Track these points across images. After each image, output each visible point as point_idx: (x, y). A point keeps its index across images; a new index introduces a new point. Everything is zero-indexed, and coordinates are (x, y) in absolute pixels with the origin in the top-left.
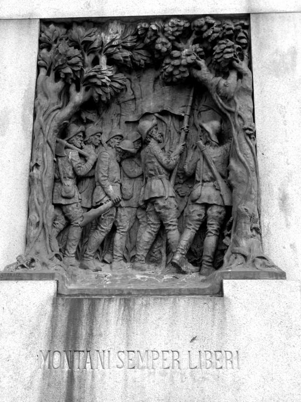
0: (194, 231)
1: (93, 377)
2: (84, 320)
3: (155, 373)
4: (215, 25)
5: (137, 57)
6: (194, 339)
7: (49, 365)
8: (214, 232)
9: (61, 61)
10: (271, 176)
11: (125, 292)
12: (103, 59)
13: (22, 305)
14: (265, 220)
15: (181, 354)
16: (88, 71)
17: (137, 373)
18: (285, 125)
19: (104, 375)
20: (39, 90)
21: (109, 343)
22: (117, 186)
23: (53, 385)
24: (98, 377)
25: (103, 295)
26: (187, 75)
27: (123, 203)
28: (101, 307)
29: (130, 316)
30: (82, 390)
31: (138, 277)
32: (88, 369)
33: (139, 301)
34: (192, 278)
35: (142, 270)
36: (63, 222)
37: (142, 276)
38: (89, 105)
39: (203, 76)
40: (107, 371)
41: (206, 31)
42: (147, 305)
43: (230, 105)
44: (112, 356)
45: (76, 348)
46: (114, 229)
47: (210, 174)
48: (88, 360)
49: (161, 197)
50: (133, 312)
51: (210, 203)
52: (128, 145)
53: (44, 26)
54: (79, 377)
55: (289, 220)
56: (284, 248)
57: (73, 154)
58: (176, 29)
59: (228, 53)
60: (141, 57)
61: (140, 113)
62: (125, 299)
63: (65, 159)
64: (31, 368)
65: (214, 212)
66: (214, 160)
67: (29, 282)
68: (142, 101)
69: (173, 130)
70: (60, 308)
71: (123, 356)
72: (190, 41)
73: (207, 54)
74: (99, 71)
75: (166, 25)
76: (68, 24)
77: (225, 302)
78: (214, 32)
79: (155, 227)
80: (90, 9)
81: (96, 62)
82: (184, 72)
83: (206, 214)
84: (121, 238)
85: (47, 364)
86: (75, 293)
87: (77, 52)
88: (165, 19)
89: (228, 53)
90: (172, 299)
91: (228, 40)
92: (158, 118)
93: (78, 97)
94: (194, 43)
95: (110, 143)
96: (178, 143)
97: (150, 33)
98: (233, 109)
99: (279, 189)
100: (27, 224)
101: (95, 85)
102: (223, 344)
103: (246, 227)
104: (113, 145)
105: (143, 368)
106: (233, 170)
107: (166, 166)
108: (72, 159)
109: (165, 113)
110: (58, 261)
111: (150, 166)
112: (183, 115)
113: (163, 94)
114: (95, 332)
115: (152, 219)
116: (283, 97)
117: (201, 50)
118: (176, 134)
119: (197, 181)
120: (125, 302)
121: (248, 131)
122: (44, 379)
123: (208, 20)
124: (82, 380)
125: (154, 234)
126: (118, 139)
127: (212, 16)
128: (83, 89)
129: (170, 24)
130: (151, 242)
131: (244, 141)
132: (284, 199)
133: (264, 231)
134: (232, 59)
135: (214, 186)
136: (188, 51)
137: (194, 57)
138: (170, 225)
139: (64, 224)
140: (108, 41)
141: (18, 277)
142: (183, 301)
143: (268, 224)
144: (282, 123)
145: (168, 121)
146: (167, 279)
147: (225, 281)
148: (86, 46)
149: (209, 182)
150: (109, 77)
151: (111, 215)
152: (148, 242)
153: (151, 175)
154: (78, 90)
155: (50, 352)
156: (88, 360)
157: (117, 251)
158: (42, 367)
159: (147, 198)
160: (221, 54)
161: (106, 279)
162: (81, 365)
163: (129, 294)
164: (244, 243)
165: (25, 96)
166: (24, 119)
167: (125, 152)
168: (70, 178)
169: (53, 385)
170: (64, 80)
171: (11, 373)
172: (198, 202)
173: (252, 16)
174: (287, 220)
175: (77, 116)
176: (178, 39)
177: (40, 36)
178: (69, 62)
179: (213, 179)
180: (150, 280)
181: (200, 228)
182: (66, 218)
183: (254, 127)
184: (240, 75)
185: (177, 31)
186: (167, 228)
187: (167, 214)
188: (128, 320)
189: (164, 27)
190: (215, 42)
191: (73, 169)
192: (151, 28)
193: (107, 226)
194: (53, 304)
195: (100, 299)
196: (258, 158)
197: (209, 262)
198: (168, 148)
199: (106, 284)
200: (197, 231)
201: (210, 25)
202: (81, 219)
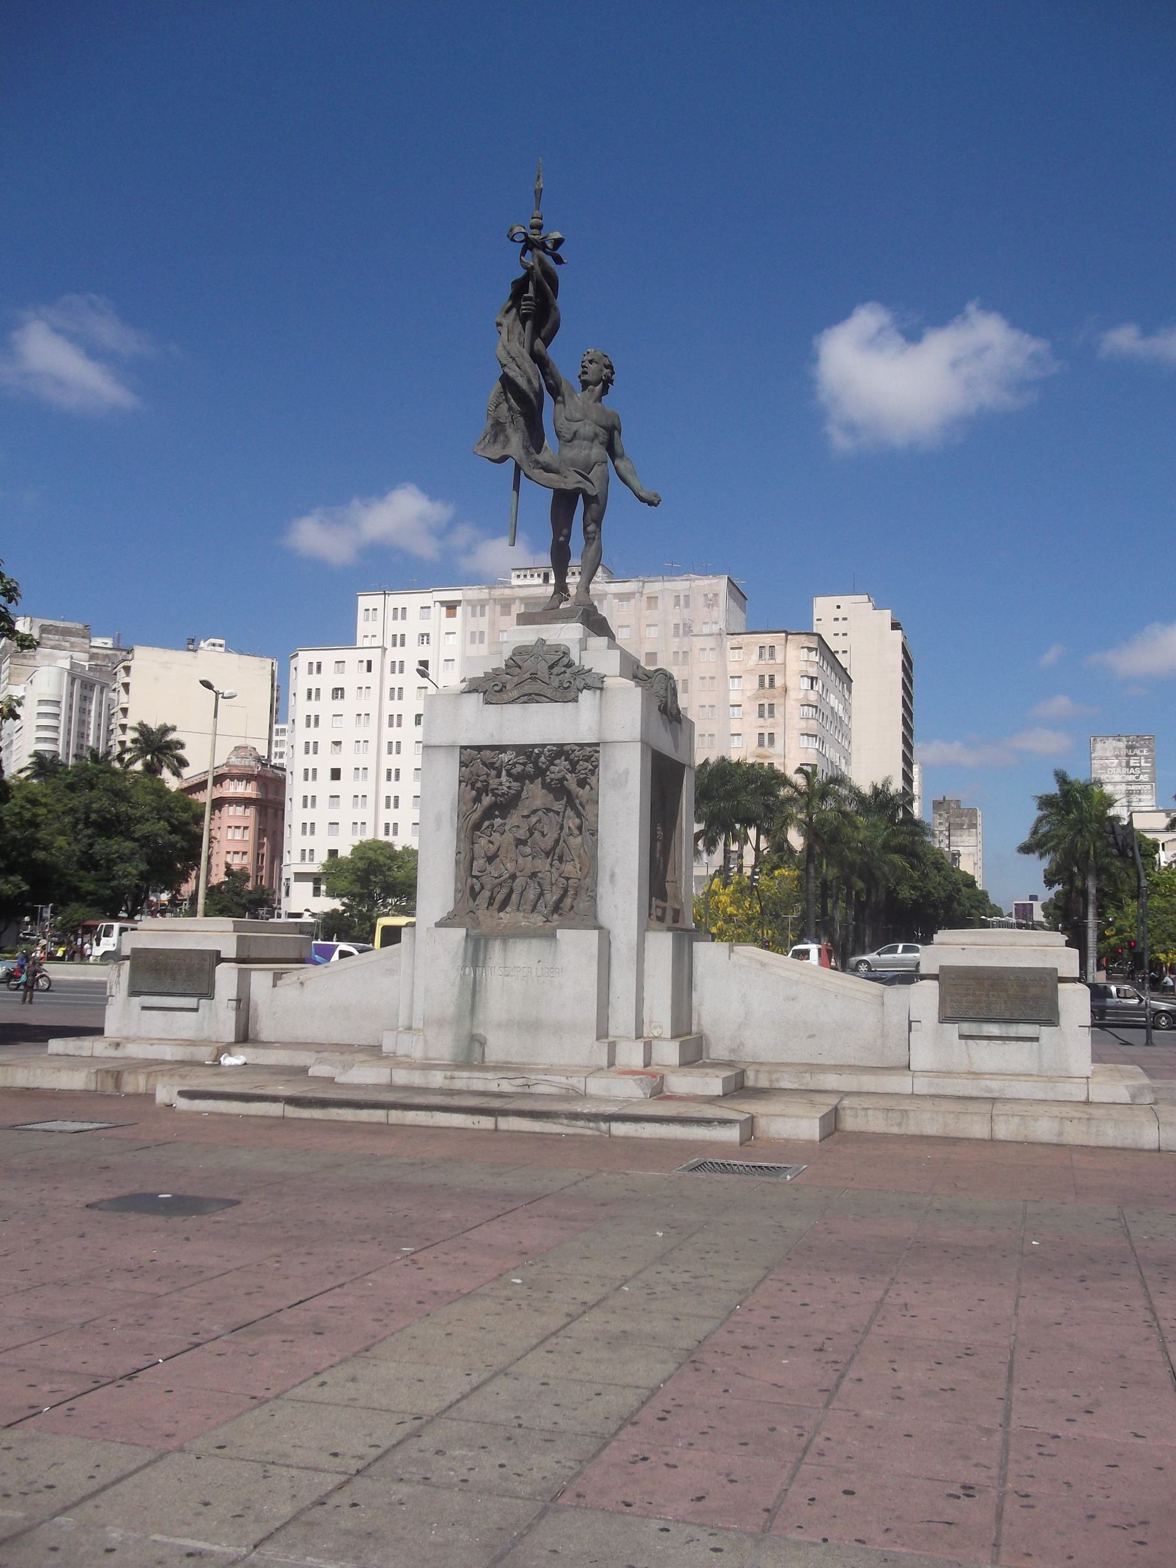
2: (482, 951)
12: (504, 773)
14: (600, 890)
27: (518, 874)
33: (511, 941)
38: (493, 806)
46: (512, 891)
52: (522, 834)
57: (483, 841)
60: (530, 768)
64: (455, 975)
74: (501, 784)
81: (499, 776)
88: (544, 746)
93: (487, 800)
132: (612, 876)
155: (464, 967)
167: (518, 839)
175: (488, 814)
188: (505, 951)
193: (505, 891)
201: (573, 751)
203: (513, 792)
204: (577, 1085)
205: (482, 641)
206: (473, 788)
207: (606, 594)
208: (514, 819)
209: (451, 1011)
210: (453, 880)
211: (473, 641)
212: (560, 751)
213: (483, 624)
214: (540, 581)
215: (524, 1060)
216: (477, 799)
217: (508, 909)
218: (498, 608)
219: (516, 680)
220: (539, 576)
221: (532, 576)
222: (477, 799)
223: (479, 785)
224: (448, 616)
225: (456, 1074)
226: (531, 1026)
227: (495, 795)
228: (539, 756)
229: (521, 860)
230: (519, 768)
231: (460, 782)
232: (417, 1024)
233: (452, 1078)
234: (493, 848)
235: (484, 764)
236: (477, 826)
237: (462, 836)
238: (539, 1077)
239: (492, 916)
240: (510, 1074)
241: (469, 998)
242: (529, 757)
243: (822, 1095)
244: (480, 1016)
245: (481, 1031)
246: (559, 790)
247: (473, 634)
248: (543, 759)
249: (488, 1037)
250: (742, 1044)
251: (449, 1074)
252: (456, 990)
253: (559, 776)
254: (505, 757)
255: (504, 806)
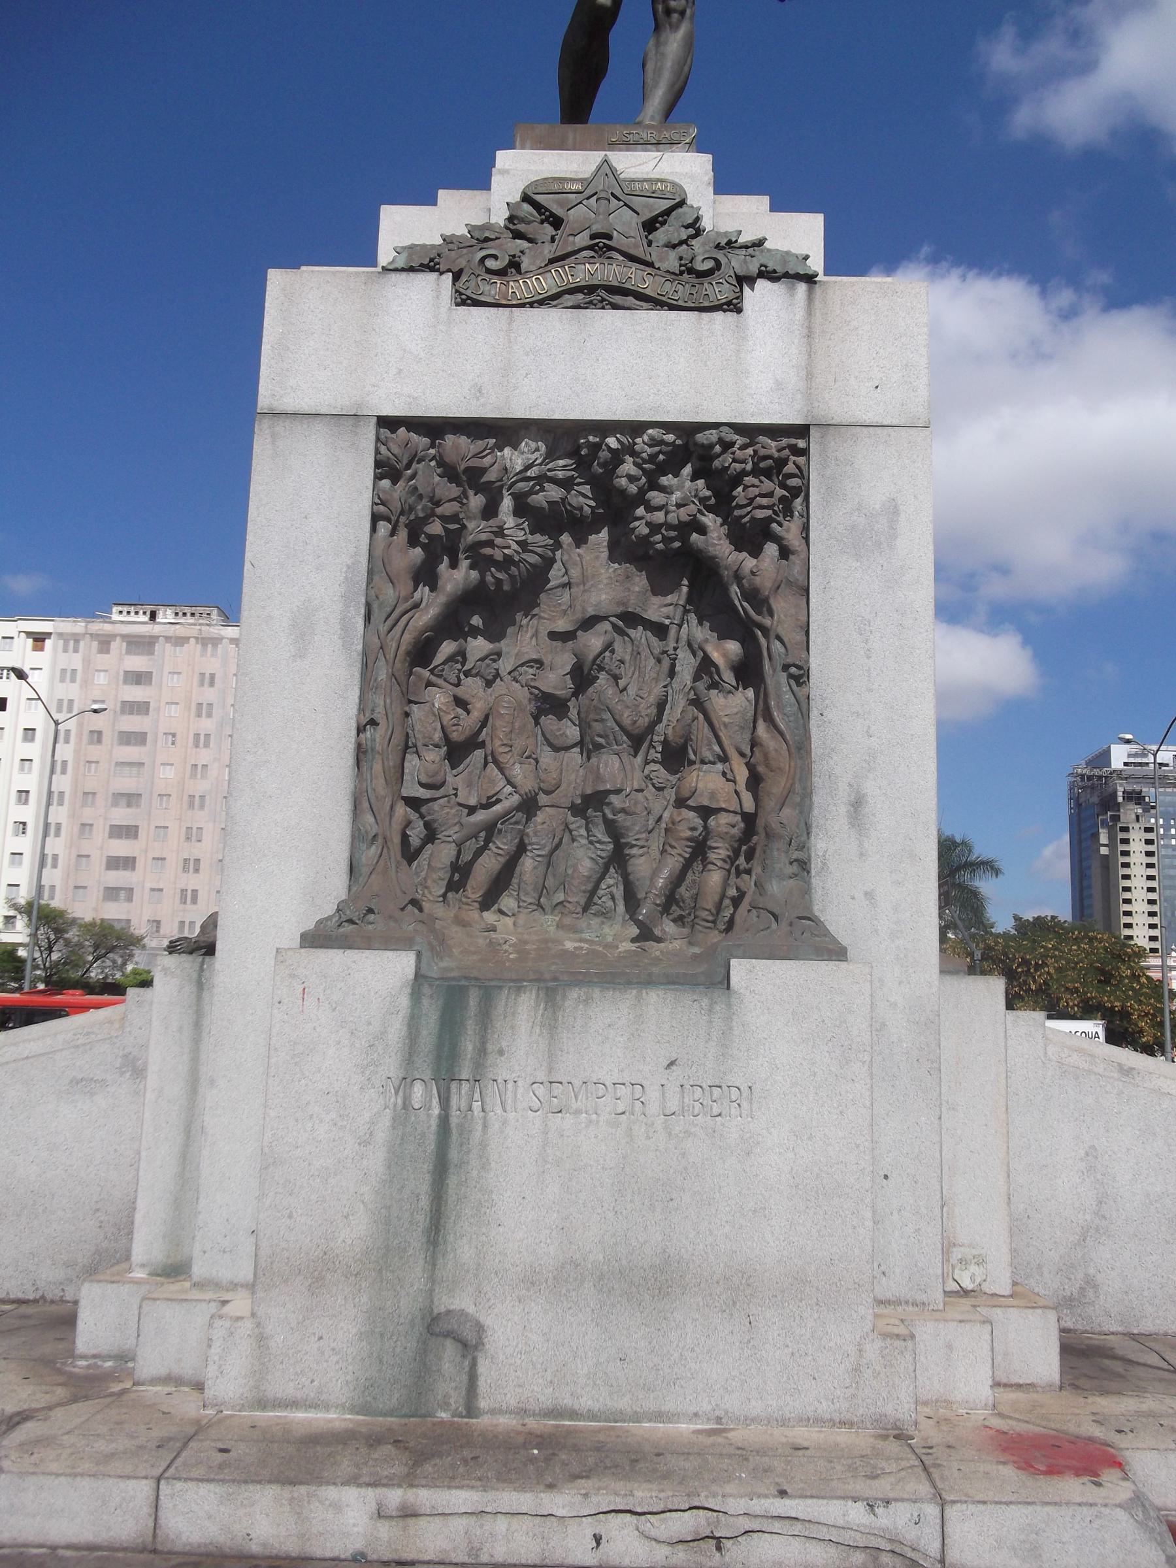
0: (681, 859)
1: (485, 1126)
2: (471, 1026)
3: (598, 1122)
4: (737, 446)
5: (575, 500)
6: (672, 1063)
7: (404, 1103)
8: (719, 863)
9: (423, 509)
10: (835, 758)
11: (547, 976)
12: (507, 503)
13: (354, 994)
14: (819, 845)
15: (646, 1089)
16: (477, 529)
17: (567, 1122)
18: (869, 657)
19: (505, 1122)
20: (377, 567)
21: (517, 1068)
22: (530, 764)
23: (412, 1138)
24: (495, 1126)
25: (504, 980)
26: (677, 544)
27: (543, 799)
28: (503, 1003)
29: (556, 1020)
30: (464, 1148)
31: (569, 945)
32: (476, 1113)
33: (574, 994)
34: (673, 938)
35: (576, 932)
36: (420, 832)
37: (577, 944)
38: (469, 600)
39: (711, 549)
40: (511, 1116)
41: (719, 456)
42: (587, 1001)
43: (759, 613)
44: (520, 1090)
45: (454, 1074)
47: (717, 748)
48: (477, 1096)
49: (618, 792)
50: (561, 1013)
51: (714, 806)
52: (556, 680)
53: (385, 432)
54: (461, 1126)
55: (866, 845)
56: (853, 898)
58: (657, 449)
59: (762, 507)
60: (583, 499)
61: (579, 616)
62: (547, 988)
63: (426, 707)
64: (372, 1108)
65: (721, 823)
66: (726, 720)
67: (368, 952)
68: (585, 591)
69: (645, 652)
70: (425, 1002)
71: (541, 1090)
72: (687, 470)
73: (722, 504)
74: (500, 532)
75: (639, 440)
76: (434, 428)
77: (732, 1000)
78: (734, 461)
79: (604, 847)
80: (482, 400)
81: (490, 511)
82: (673, 540)
83: (705, 827)
84: (535, 868)
85: (400, 1101)
86: (452, 975)
87: (454, 490)
88: (636, 428)
89: (762, 507)
90: (634, 992)
91: (762, 478)
92: (614, 626)
93: (456, 577)
94: (694, 477)
95: (516, 674)
96: (657, 680)
97: (604, 455)
98: (767, 622)
99: (850, 785)
100: (353, 837)
101: (490, 560)
102: (724, 1073)
103: (780, 859)
104: (523, 679)
105: (578, 1112)
106: (761, 745)
107: (630, 728)
108: (439, 709)
109: (631, 619)
110: (416, 911)
111: (597, 727)
112: (667, 622)
113: (628, 577)
114: (490, 1047)
115: (600, 833)
116: (867, 602)
117: (708, 493)
118: (652, 661)
119: (689, 760)
120: (547, 994)
121: (793, 670)
122: (394, 1128)
123: (723, 434)
124: (465, 1131)
125: (601, 861)
126: (532, 667)
127: (733, 426)
128: (465, 564)
129: (646, 438)
130: (596, 877)
131: (786, 689)
132: (857, 804)
133: (814, 868)
134: (769, 520)
135: (724, 774)
136: (683, 487)
137: (692, 509)
138: (633, 846)
139: (422, 836)
140: (519, 468)
141: (345, 943)
142: (655, 996)
143: (825, 852)
144: (862, 652)
145: (638, 633)
146: (625, 951)
147: (733, 962)
148: (471, 478)
149: (714, 763)
150: (517, 542)
151: (516, 823)
152: (589, 877)
153: (598, 747)
154: (454, 565)
155: (406, 1081)
156: (477, 1096)
157: (527, 894)
158: (391, 1106)
159: (589, 792)
160: (749, 509)
161: (506, 947)
162: (463, 1105)
163: (555, 979)
164: (776, 888)
165: (346, 578)
166: (345, 626)
168: (436, 746)
169: (412, 1138)
170: (425, 547)
171: (333, 1115)
172: (690, 803)
173: (812, 431)
174: (861, 845)
175: (452, 623)
176: (662, 470)
177: (377, 452)
178: (439, 511)
179: (724, 759)
180: (594, 952)
181: (691, 854)
182: (427, 825)
183: (807, 661)
184: (785, 553)
185: (660, 452)
186: (627, 851)
187: (628, 824)
188: (551, 1027)
189: (635, 444)
190: (737, 480)
191: (443, 728)
192: (607, 445)
193: (503, 845)
194: (412, 994)
195: (500, 988)
196: (812, 722)
197: (708, 921)
198: (635, 689)
199: (509, 960)
200: (685, 859)
201: (727, 446)
202: (456, 828)
203: (532, 559)
204: (910, 1534)
205: (73, 680)
206: (413, 541)
207: (221, 639)
208: (524, 641)
209: (354, 1232)
210: (346, 807)
211: (62, 680)
212: (689, 446)
213: (76, 661)
214: (146, 618)
215: (623, 1403)
216: (426, 575)
217: (507, 902)
218: (95, 644)
219: (548, 251)
220: (145, 613)
221: (137, 613)
222: (426, 575)
223: (436, 528)
224: (35, 649)
225: (423, 1497)
226: (647, 1284)
227: (480, 562)
228: (617, 458)
229: (547, 757)
230: (554, 493)
231: (375, 518)
232: (219, 1255)
233: (408, 1513)
234: (468, 722)
235: (450, 472)
236: (422, 653)
237: (383, 675)
238: (759, 1506)
239: (464, 924)
240: (643, 1495)
241: (423, 1186)
242: (582, 465)
243: (1142, 1368)
244: (462, 1251)
245: (462, 1302)
246: (676, 563)
247: (64, 671)
248: (628, 466)
249: (487, 1321)
250: (1090, 1283)
251: (395, 1497)
252: (376, 1160)
253: (684, 514)
254: (515, 458)
255: (500, 602)
